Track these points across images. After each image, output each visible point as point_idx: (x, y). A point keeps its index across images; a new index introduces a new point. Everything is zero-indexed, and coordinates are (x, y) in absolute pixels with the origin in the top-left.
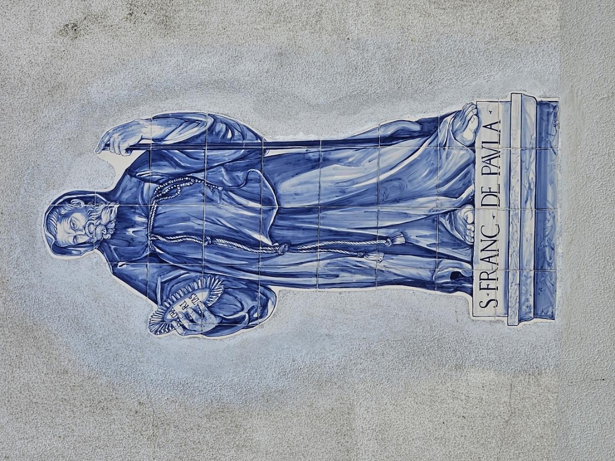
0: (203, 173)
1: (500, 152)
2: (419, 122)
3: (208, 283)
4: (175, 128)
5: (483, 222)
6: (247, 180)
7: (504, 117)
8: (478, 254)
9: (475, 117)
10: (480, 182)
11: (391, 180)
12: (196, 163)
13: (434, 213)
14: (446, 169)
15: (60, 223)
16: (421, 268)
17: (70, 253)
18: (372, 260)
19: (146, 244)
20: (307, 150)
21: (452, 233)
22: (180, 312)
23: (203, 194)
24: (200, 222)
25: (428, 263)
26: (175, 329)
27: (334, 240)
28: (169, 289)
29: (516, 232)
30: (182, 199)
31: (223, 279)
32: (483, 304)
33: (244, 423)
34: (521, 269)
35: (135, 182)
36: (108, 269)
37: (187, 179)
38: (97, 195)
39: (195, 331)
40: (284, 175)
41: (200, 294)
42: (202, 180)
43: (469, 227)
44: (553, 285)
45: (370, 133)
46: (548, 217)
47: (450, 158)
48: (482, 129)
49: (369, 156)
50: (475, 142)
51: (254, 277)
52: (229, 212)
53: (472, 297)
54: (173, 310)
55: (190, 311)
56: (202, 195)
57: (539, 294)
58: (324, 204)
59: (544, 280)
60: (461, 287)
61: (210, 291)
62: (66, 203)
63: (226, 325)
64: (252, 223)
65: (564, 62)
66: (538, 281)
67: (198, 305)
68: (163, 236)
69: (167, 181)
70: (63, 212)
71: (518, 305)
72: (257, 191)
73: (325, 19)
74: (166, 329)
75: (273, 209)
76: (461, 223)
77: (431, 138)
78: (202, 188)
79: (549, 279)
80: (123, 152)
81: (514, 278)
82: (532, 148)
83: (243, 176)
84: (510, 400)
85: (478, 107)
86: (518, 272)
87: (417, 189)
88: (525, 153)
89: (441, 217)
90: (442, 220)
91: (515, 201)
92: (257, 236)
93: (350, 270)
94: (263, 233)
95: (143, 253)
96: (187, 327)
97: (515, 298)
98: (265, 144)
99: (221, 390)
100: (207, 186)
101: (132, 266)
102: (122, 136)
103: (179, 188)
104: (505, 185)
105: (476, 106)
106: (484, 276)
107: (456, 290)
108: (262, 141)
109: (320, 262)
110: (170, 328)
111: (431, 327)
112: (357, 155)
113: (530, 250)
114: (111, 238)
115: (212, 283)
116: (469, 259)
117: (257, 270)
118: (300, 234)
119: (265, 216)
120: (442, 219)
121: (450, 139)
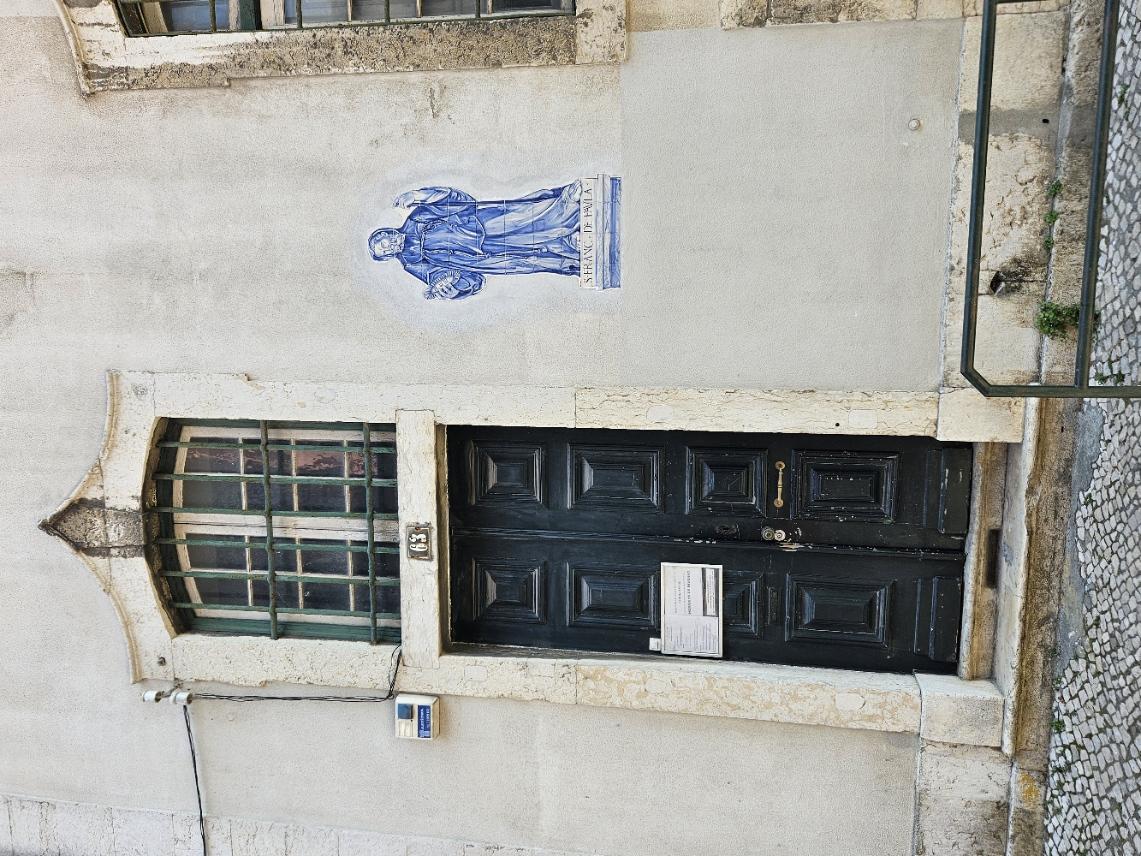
5: (583, 240)
8: (583, 256)
10: (582, 223)
17: (382, 260)
18: (532, 260)
51: (474, 270)
52: (461, 237)
92: (475, 249)
118: (496, 248)
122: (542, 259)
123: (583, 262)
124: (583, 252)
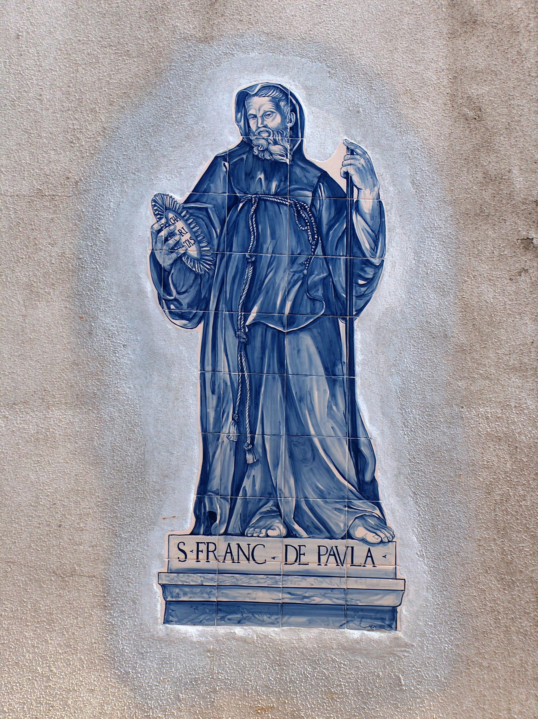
0: (322, 254)
1: (343, 565)
2: (374, 480)
3: (206, 257)
4: (370, 224)
5: (270, 549)
6: (313, 300)
7: (379, 571)
8: (234, 542)
9: (380, 539)
10: (311, 544)
11: (312, 450)
12: (332, 247)
13: (278, 495)
14: (325, 508)
15: (270, 101)
16: (221, 480)
17: (238, 110)
18: (229, 430)
19: (248, 192)
20: (344, 363)
21: (258, 513)
22: (175, 227)
23: (299, 254)
24: (270, 250)
25: (226, 488)
26: (158, 221)
27: (251, 389)
28: (200, 216)
29: (258, 583)
30: (295, 232)
31: (211, 273)
32: (181, 546)
33: (57, 293)
34: (219, 587)
35: (313, 181)
36: (221, 151)
37: (316, 237)
38: (300, 141)
39: (156, 243)
40: (319, 339)
41: (195, 249)
42: (314, 252)
43: (264, 531)
44: (201, 622)
45: (362, 429)
46: (273, 617)
47: (336, 512)
48: (366, 547)
49: (338, 427)
50: (353, 539)
51: (212, 306)
52: (281, 282)
53: (190, 534)
54: (178, 219)
55: (177, 238)
56: (298, 252)
57: (191, 607)
58: (288, 378)
59: (206, 612)
60: (200, 522)
61: (197, 260)
62: (292, 108)
63: (161, 276)
64: (269, 305)
65: (439, 637)
66: (205, 606)
67: (183, 246)
68: (256, 211)
69: (313, 215)
70: (282, 104)
71: (180, 583)
72: (303, 310)
73: (483, 384)
74: (157, 212)
75: (284, 327)
76: (268, 523)
77: (357, 493)
78: (306, 253)
79: (207, 618)
80: (344, 169)
81: (209, 580)
82: (346, 601)
83: (318, 296)
84: (77, 575)
85: (390, 543)
86: (215, 584)
87: (303, 477)
88: (341, 593)
89: (274, 502)
90: (271, 503)
91: (291, 581)
92: (255, 309)
93: (219, 406)
94: (257, 316)
95: (238, 189)
96: (160, 234)
97: (188, 581)
98: (351, 320)
99: (93, 268)
100: (308, 258)
101: (224, 177)
102: (362, 168)
103: (306, 228)
104: (307, 571)
105: (391, 541)
106: (211, 547)
107: (197, 517)
108: (355, 315)
109: (228, 375)
110: (159, 216)
111: (159, 491)
112: (339, 414)
113: (238, 597)
114: (254, 155)
115: (207, 262)
116: (230, 531)
117: (220, 309)
118: (257, 354)
119: (276, 319)
120: (272, 503)
121: (356, 513)
122: (229, 453)
123: (221, 543)
124: (244, 542)
